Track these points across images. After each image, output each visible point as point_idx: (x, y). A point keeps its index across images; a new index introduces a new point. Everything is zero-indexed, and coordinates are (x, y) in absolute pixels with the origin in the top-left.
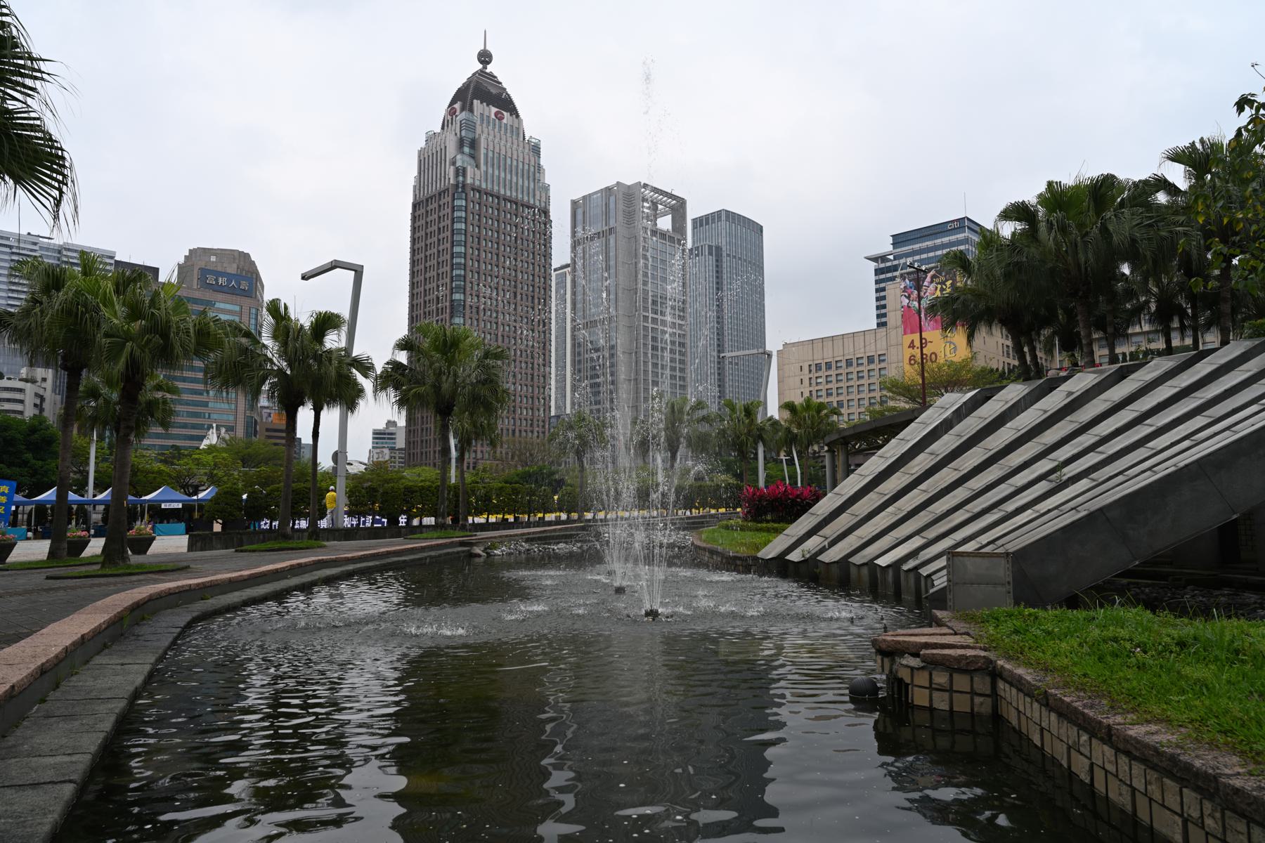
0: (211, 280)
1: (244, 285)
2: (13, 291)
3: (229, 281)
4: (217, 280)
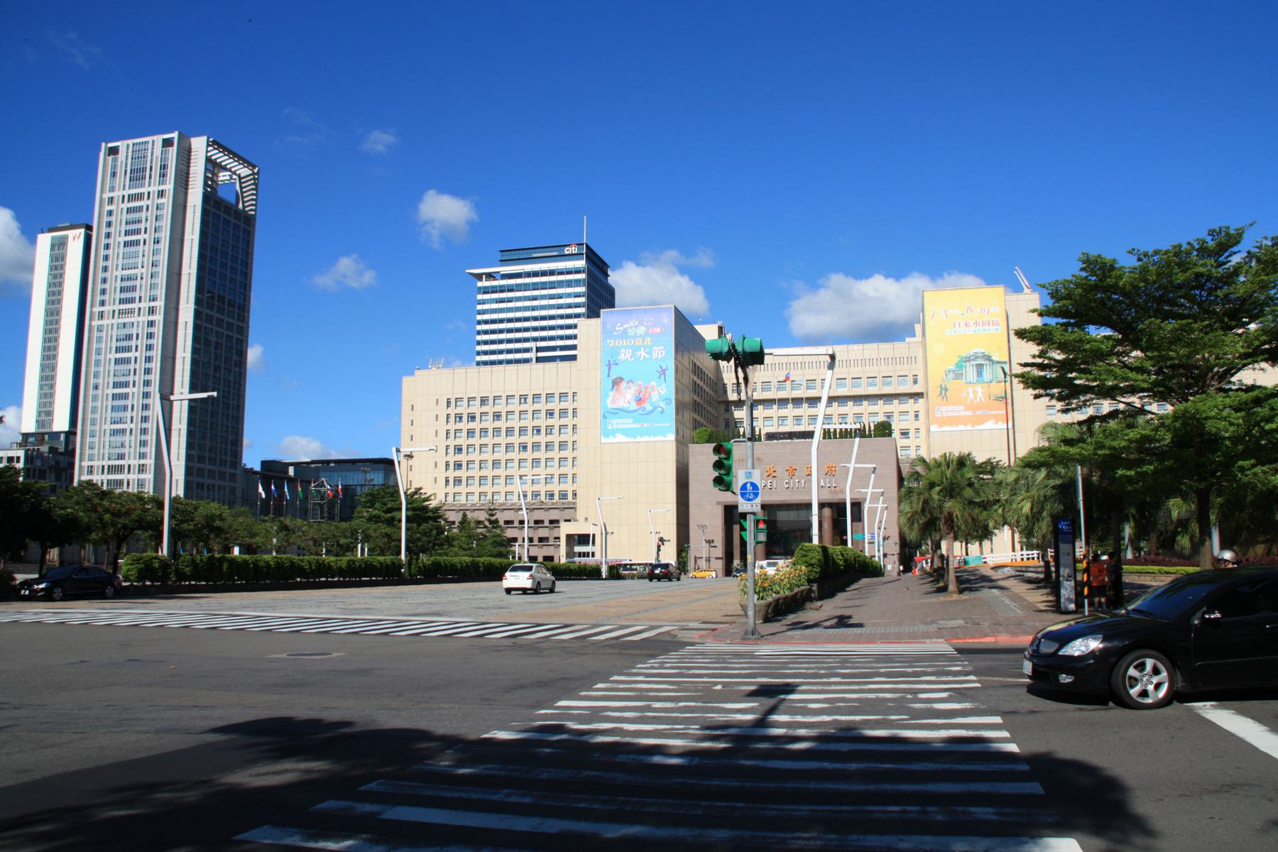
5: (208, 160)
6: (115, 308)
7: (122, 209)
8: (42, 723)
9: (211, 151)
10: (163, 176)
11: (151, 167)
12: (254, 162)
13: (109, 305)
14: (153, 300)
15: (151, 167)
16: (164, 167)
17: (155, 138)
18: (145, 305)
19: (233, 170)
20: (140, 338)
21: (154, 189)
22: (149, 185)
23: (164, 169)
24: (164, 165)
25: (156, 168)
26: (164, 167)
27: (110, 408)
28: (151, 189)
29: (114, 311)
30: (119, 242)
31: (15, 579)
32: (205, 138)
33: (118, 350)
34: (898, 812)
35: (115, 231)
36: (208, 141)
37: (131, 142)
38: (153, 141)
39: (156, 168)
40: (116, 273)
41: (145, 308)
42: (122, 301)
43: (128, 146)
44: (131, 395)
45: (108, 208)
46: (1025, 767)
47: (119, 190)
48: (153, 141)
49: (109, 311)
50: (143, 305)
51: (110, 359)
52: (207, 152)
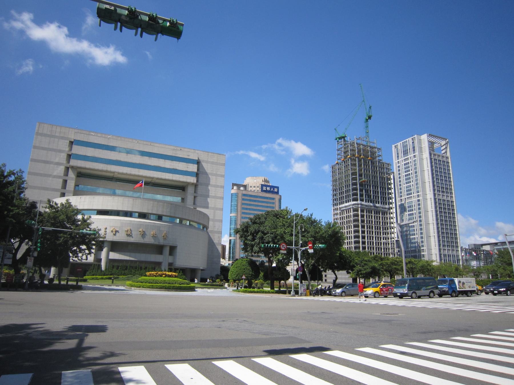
0: (264, 188)
1: (276, 190)
2: (246, 209)
3: (271, 189)
4: (266, 189)
5: (429, 141)
6: (405, 197)
7: (404, 187)
8: (403, 340)
9: (429, 138)
10: (414, 151)
11: (409, 149)
12: (445, 137)
13: (403, 196)
14: (418, 193)
15: (409, 149)
16: (414, 148)
17: (409, 139)
18: (416, 194)
19: (438, 142)
20: (415, 206)
21: (412, 155)
22: (410, 155)
23: (414, 148)
24: (414, 147)
25: (411, 148)
26: (414, 148)
27: (406, 191)
28: (411, 156)
29: (402, 160)
30: (403, 175)
31: (319, 267)
32: (426, 134)
33: (405, 172)
34: (18, 333)
35: (403, 195)
36: (427, 135)
37: (401, 142)
38: (409, 140)
39: (411, 148)
40: (404, 186)
41: (415, 196)
42: (407, 195)
43: (401, 143)
44: (415, 226)
45: (398, 165)
46: (421, 297)
47: (400, 158)
48: (409, 140)
49: (404, 199)
50: (414, 195)
51: (403, 175)
52: (428, 138)
